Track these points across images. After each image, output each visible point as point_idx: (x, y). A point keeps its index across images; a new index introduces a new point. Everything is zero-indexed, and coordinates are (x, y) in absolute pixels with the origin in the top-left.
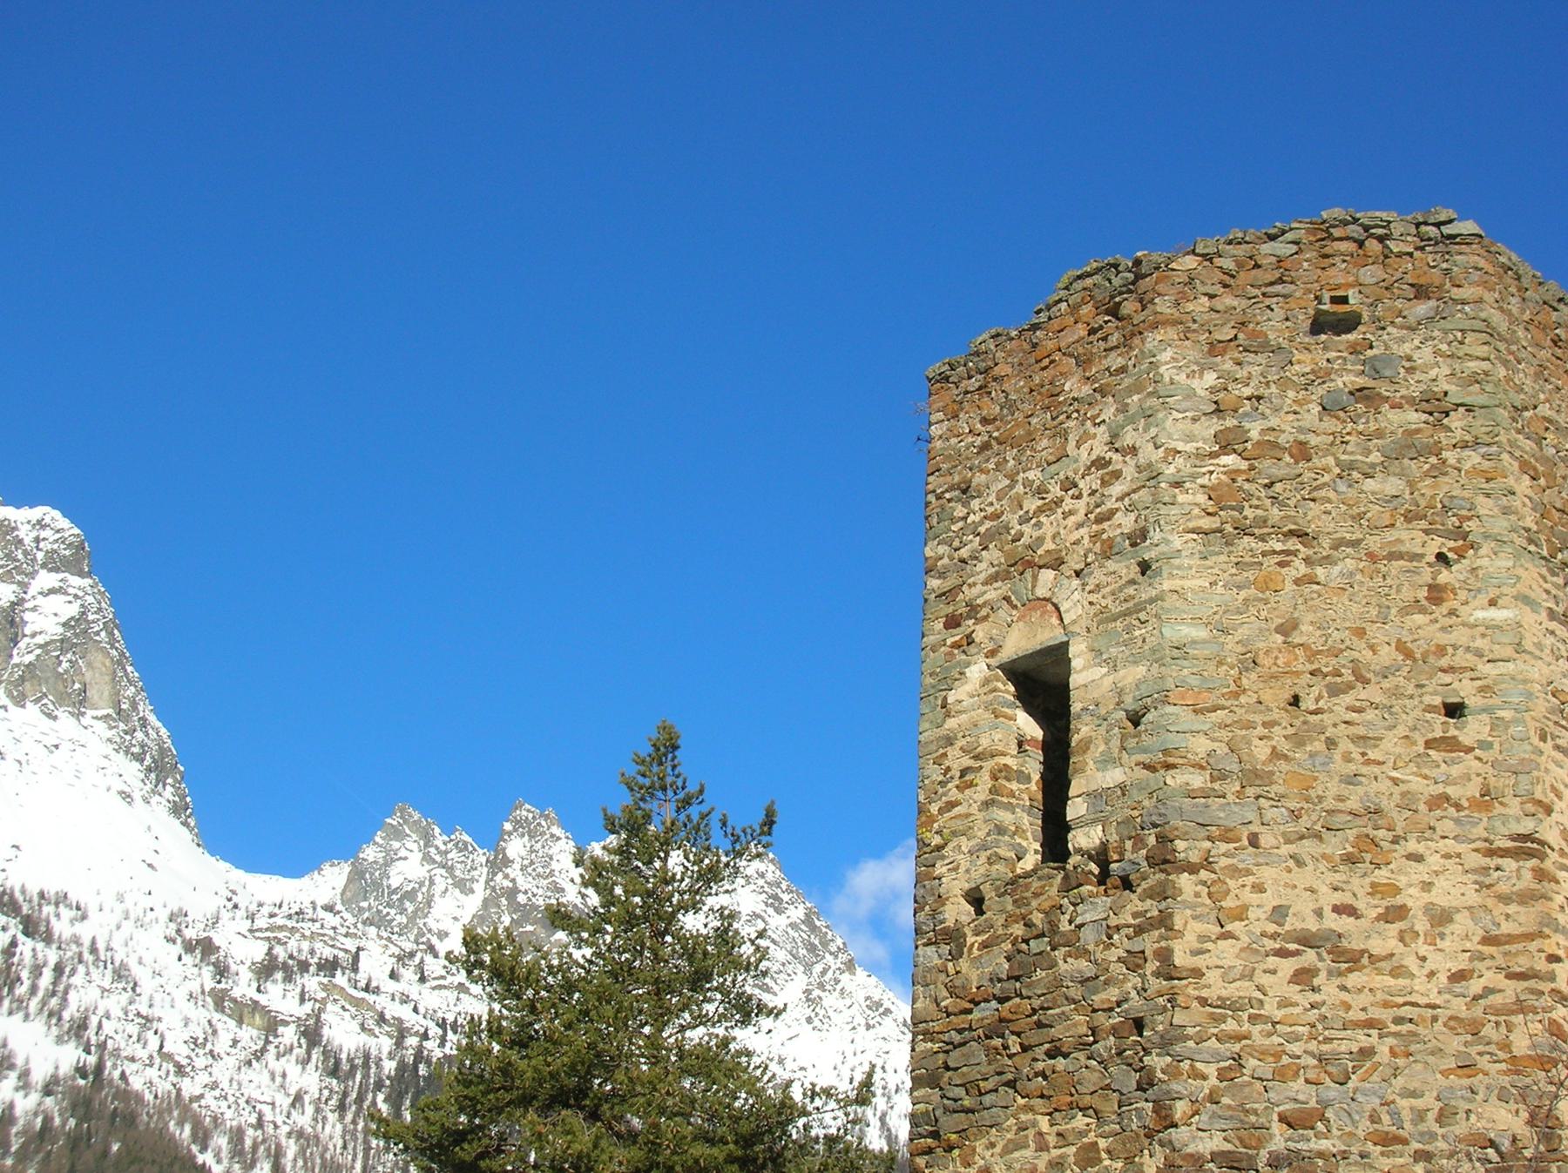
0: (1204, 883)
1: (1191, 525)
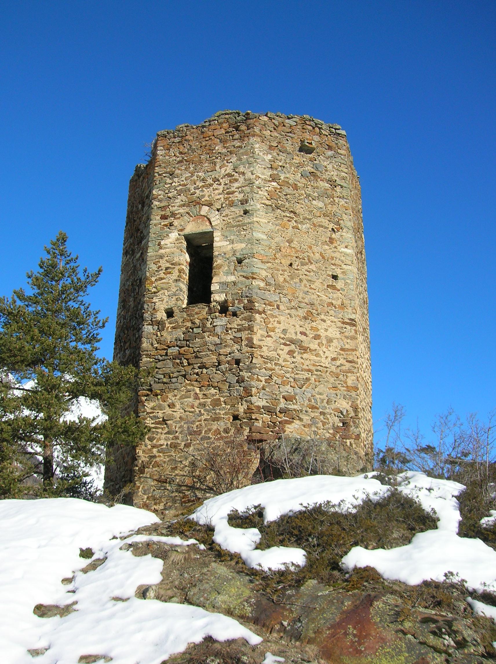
0: (263, 318)
1: (263, 202)
